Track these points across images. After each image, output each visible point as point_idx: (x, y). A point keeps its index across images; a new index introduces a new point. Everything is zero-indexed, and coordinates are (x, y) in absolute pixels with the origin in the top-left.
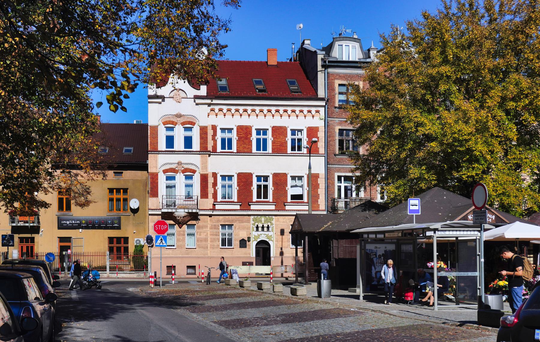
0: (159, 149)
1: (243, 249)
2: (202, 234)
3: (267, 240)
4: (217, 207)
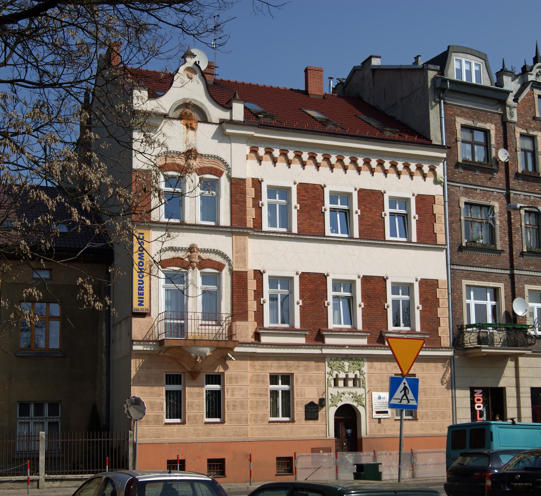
0: (354, 237)
1: (311, 422)
2: (236, 392)
3: (355, 404)
4: (264, 339)
